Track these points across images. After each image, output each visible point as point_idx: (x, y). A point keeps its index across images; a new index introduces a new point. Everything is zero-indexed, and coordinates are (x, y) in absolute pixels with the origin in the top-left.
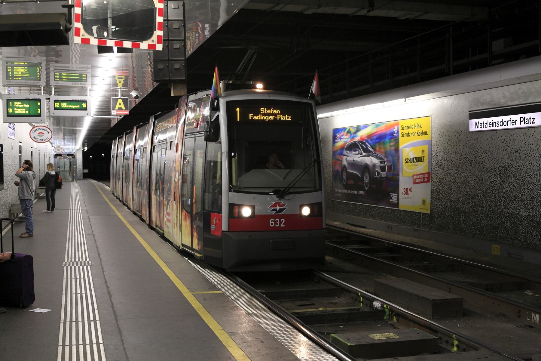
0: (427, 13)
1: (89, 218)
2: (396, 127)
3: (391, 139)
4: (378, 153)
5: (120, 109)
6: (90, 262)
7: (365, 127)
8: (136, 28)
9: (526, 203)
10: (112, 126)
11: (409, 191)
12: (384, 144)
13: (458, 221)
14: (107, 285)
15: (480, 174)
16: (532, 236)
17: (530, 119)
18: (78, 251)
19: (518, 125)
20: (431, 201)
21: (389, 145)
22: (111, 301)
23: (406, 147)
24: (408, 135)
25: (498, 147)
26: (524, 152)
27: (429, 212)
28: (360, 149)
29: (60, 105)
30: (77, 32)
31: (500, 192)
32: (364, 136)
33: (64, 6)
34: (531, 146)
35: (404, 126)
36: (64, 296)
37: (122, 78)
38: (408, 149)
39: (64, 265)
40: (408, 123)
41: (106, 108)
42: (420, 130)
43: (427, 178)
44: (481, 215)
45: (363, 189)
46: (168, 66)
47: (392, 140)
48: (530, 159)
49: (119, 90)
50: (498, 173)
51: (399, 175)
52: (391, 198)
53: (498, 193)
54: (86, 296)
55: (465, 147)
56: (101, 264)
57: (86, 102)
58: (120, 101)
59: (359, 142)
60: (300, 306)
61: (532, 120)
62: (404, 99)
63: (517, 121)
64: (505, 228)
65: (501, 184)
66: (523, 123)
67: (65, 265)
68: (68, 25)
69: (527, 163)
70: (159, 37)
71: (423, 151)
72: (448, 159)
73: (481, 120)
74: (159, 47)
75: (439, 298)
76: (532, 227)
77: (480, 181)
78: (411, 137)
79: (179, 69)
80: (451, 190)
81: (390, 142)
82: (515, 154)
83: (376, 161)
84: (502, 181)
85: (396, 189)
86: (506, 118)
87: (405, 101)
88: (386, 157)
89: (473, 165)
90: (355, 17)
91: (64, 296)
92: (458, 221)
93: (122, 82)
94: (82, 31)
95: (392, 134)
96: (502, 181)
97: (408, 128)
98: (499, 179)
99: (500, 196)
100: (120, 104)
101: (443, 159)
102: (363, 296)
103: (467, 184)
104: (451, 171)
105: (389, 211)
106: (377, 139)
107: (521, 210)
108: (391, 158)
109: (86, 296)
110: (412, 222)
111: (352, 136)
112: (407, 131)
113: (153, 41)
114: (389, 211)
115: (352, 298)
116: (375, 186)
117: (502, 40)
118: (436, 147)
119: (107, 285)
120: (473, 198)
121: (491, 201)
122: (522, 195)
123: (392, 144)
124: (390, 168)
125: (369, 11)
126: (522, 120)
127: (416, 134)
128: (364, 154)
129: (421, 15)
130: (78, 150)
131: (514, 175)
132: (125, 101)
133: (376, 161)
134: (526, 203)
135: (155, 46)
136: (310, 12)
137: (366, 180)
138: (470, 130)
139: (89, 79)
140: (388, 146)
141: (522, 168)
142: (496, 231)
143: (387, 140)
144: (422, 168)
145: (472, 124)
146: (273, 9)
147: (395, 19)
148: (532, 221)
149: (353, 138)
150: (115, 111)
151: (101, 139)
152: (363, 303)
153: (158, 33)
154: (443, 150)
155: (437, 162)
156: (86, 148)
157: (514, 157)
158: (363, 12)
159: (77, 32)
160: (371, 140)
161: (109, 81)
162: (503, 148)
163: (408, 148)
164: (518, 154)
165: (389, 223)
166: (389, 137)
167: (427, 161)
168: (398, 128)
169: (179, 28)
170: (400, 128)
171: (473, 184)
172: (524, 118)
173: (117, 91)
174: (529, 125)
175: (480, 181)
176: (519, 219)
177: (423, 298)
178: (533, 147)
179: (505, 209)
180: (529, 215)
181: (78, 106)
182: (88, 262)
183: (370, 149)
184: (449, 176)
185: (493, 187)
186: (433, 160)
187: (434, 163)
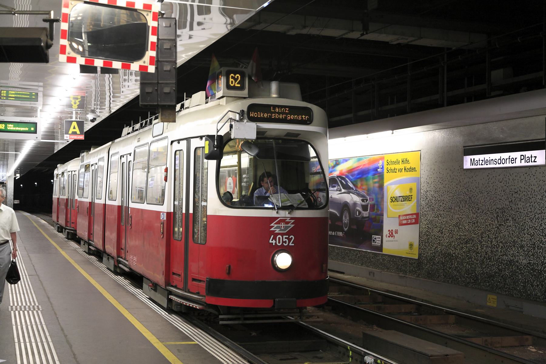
0: (353, 31)
1: (29, 256)
2: (381, 162)
3: (374, 175)
4: (360, 190)
5: (74, 133)
6: (40, 307)
7: (346, 160)
8: (110, 45)
9: (526, 249)
10: (55, 152)
11: (394, 233)
12: (367, 180)
13: (450, 268)
14: (64, 334)
15: (475, 216)
16: (532, 286)
17: (531, 157)
18: (24, 294)
19: (518, 164)
20: (419, 245)
21: (372, 182)
22: (72, 351)
23: (391, 184)
24: (394, 171)
25: (495, 187)
26: (525, 193)
27: (417, 258)
28: (339, 186)
29: (6, 127)
30: (63, 50)
31: (498, 237)
32: (344, 171)
33: (45, 21)
34: (532, 187)
35: (389, 160)
36: (17, 345)
37: (77, 99)
38: (393, 186)
39: (10, 310)
40: (394, 158)
41: (51, 133)
42: (408, 166)
43: (415, 219)
44: (475, 261)
45: (342, 231)
46: (157, 90)
47: (376, 176)
48: (530, 201)
49: (74, 112)
50: (495, 215)
51: (383, 215)
52: (374, 241)
53: (495, 238)
54: (43, 345)
55: (459, 187)
56: (53, 310)
57: (35, 124)
58: (74, 124)
59: (338, 177)
60: (281, 360)
61: (533, 159)
62: (391, 131)
63: (517, 159)
64: (502, 276)
65: (498, 228)
66: (523, 161)
67: (12, 310)
68: (50, 42)
69: (528, 205)
70: (152, 58)
71: (411, 189)
72: (439, 199)
73: (476, 157)
74: (152, 69)
75: (437, 354)
76: (532, 276)
77: (474, 223)
78: (398, 173)
79: (169, 93)
80: (442, 233)
81: (373, 179)
82: (514, 195)
83: (357, 199)
84: (500, 225)
85: (380, 231)
86: (505, 155)
87: (393, 133)
88: (368, 195)
89: (467, 206)
90: (342, 41)
91: (17, 345)
92: (450, 268)
93: (78, 103)
94: (68, 49)
95: (376, 169)
96: (500, 225)
97: (397, 162)
98: (496, 222)
99: (497, 242)
100: (74, 128)
101: (434, 199)
102: (352, 349)
103: (460, 227)
104: (442, 213)
105: (371, 255)
106: (358, 174)
107: (521, 257)
108: (374, 196)
109: (43, 345)
110: (397, 268)
111: (331, 170)
112: (393, 167)
113: (144, 62)
114: (371, 255)
115: (340, 352)
116: (355, 227)
117: (502, 70)
118: (426, 185)
119: (64, 334)
120: (466, 243)
121: (487, 247)
122: (521, 241)
123: (376, 180)
124: (373, 207)
125: (362, 35)
126: (523, 158)
127: (403, 170)
128: (343, 191)
129: (414, 40)
130: (9, 177)
131: (513, 218)
132: (81, 124)
133: (357, 199)
134: (526, 249)
135: (146, 68)
136: (293, 33)
137: (346, 220)
138: (465, 168)
139: (40, 98)
140: (371, 182)
141: (522, 211)
142: (492, 280)
143: (370, 176)
144: (409, 208)
145: (466, 161)
146: (253, 28)
147: (386, 43)
148: (532, 269)
149: (331, 172)
150: (68, 135)
151: (39, 165)
152: (352, 358)
153: (151, 53)
154: (434, 189)
155: (427, 201)
156: (18, 176)
157: (513, 199)
158: (355, 35)
159: (63, 50)
160: (352, 176)
161: (65, 101)
162: (501, 189)
163: (394, 185)
164: (518, 196)
165: (370, 269)
166: (372, 173)
167: (415, 201)
168: (383, 163)
169: (170, 49)
170: (385, 163)
171: (467, 227)
172: (524, 156)
173: (72, 113)
174: (530, 164)
175: (474, 223)
176: (518, 267)
177: (420, 353)
178: (534, 188)
179: (503, 255)
180: (530, 263)
181: (27, 129)
182: (38, 306)
183: (351, 185)
184: (440, 218)
185: (489, 231)
186: (422, 199)
187: (423, 203)
